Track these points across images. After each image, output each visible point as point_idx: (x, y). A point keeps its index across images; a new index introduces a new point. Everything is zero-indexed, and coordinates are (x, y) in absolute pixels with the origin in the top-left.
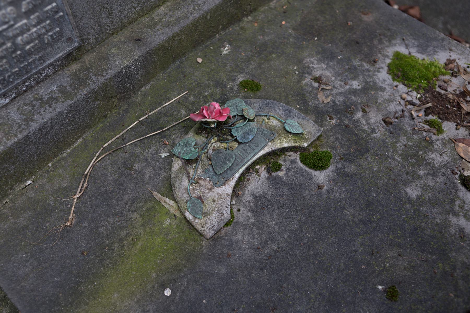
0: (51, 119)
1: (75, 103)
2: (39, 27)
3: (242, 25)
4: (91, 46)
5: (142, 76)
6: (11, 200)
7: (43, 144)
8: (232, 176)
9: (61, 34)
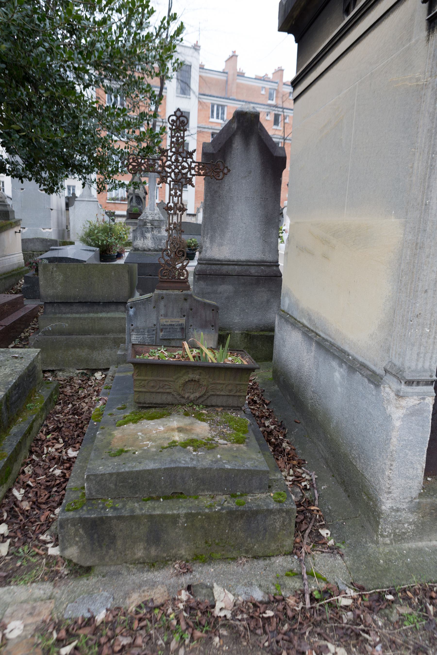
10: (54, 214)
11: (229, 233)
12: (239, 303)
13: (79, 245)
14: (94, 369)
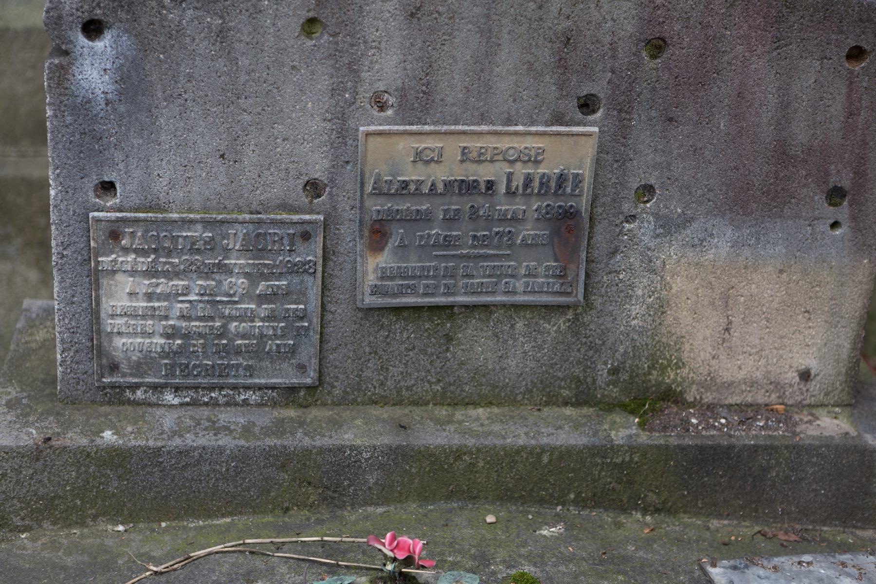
0: (204, 448)
1: (248, 448)
2: (267, 324)
3: (622, 518)
4: (332, 400)
5: (376, 483)
6: (82, 535)
7: (173, 481)
9: (294, 351)
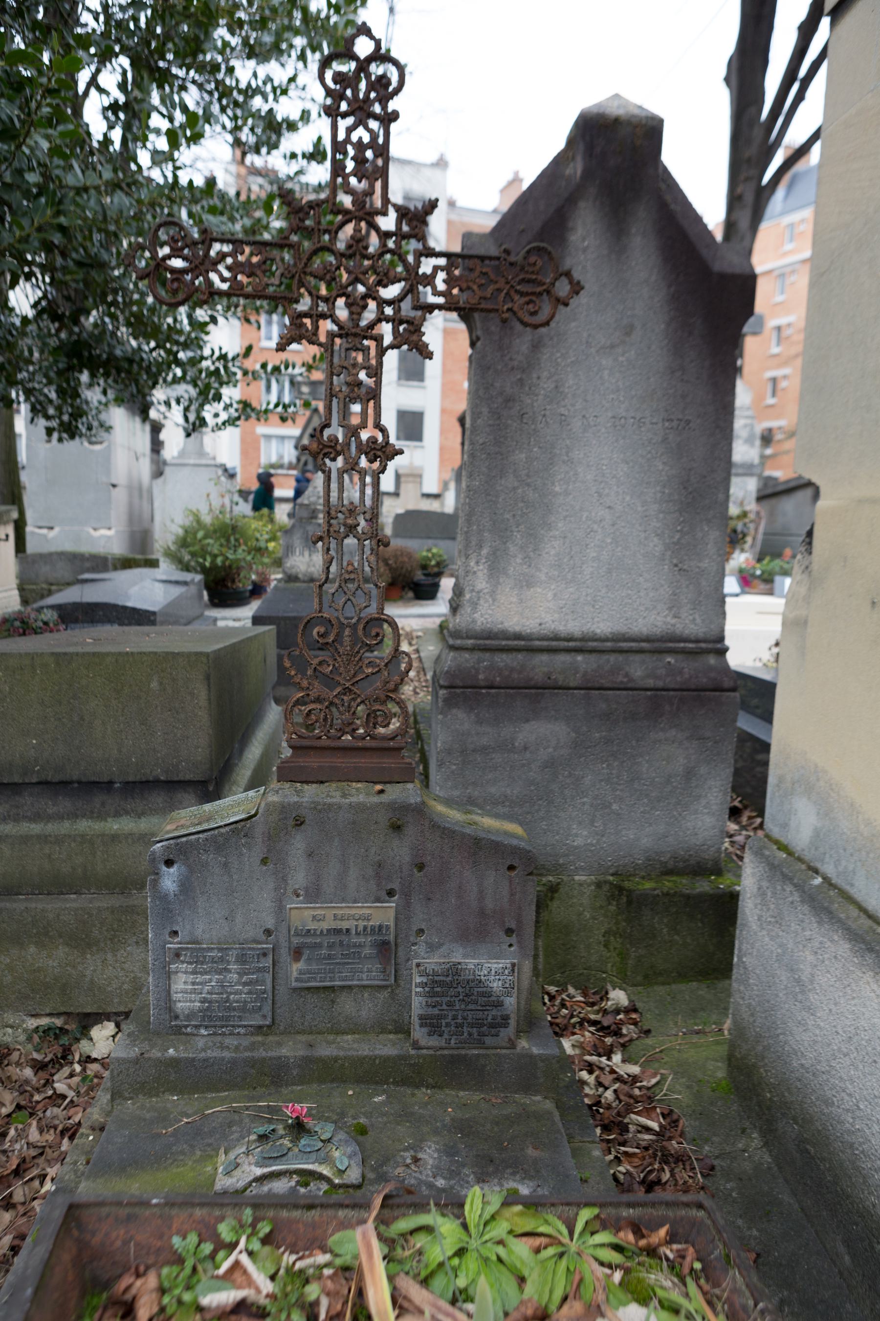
3: (416, 1092)
8: (271, 1166)
9: (260, 1008)
10: (120, 496)
11: (556, 543)
12: (588, 780)
13: (166, 569)
14: (88, 1015)
